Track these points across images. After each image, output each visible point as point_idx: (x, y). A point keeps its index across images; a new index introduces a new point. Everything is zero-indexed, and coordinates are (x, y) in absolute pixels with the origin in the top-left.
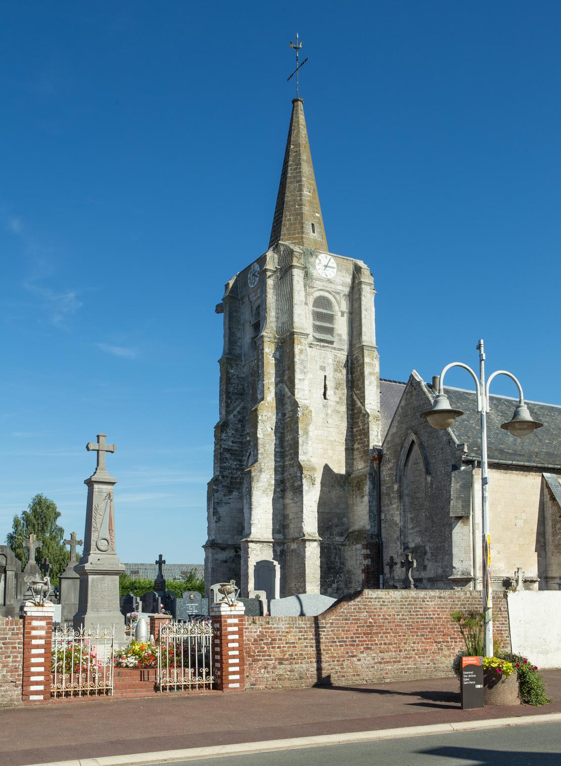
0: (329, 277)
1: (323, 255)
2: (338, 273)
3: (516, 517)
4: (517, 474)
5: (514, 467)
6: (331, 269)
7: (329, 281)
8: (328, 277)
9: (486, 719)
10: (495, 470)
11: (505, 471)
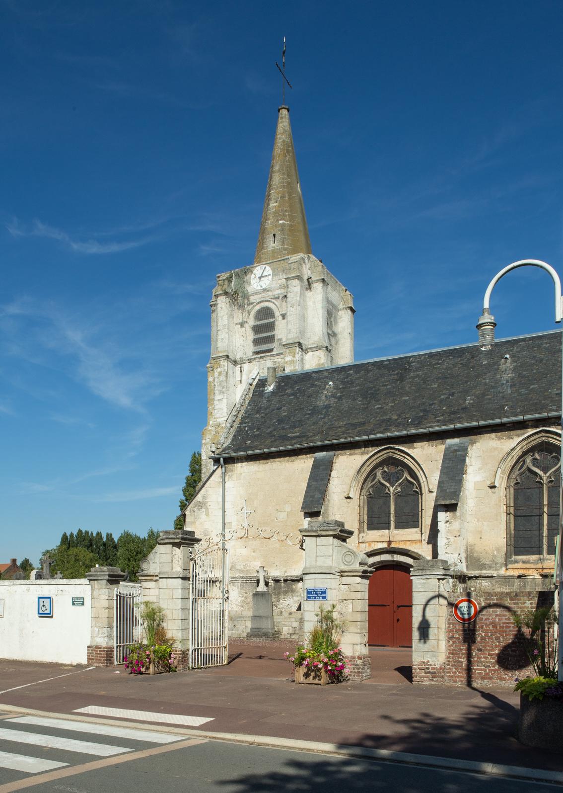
0: (264, 287)
1: (257, 268)
2: (274, 278)
3: (277, 510)
4: (280, 462)
5: (276, 454)
6: (267, 278)
7: (265, 290)
8: (263, 287)
9: (28, 708)
10: (252, 462)
11: (265, 461)
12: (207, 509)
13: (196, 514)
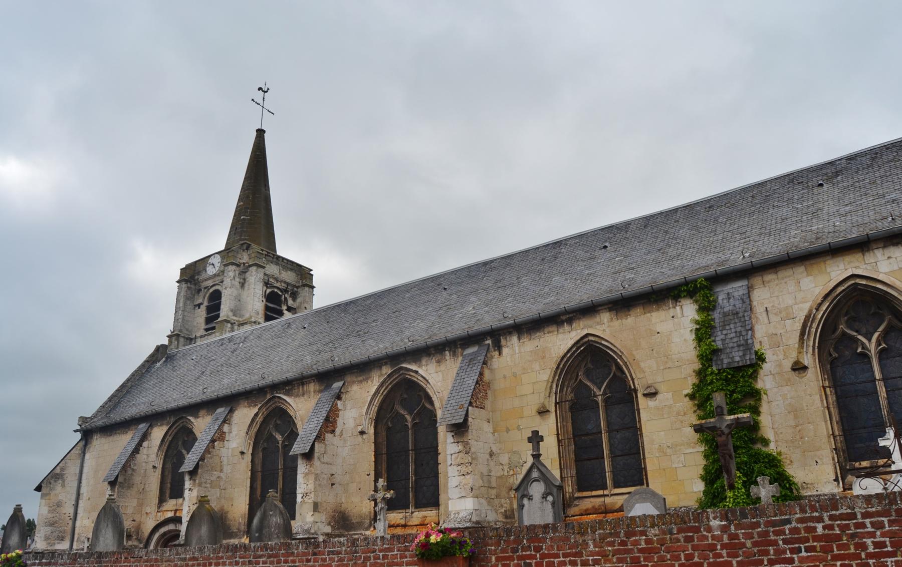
12: (64, 481)
13: (51, 486)
